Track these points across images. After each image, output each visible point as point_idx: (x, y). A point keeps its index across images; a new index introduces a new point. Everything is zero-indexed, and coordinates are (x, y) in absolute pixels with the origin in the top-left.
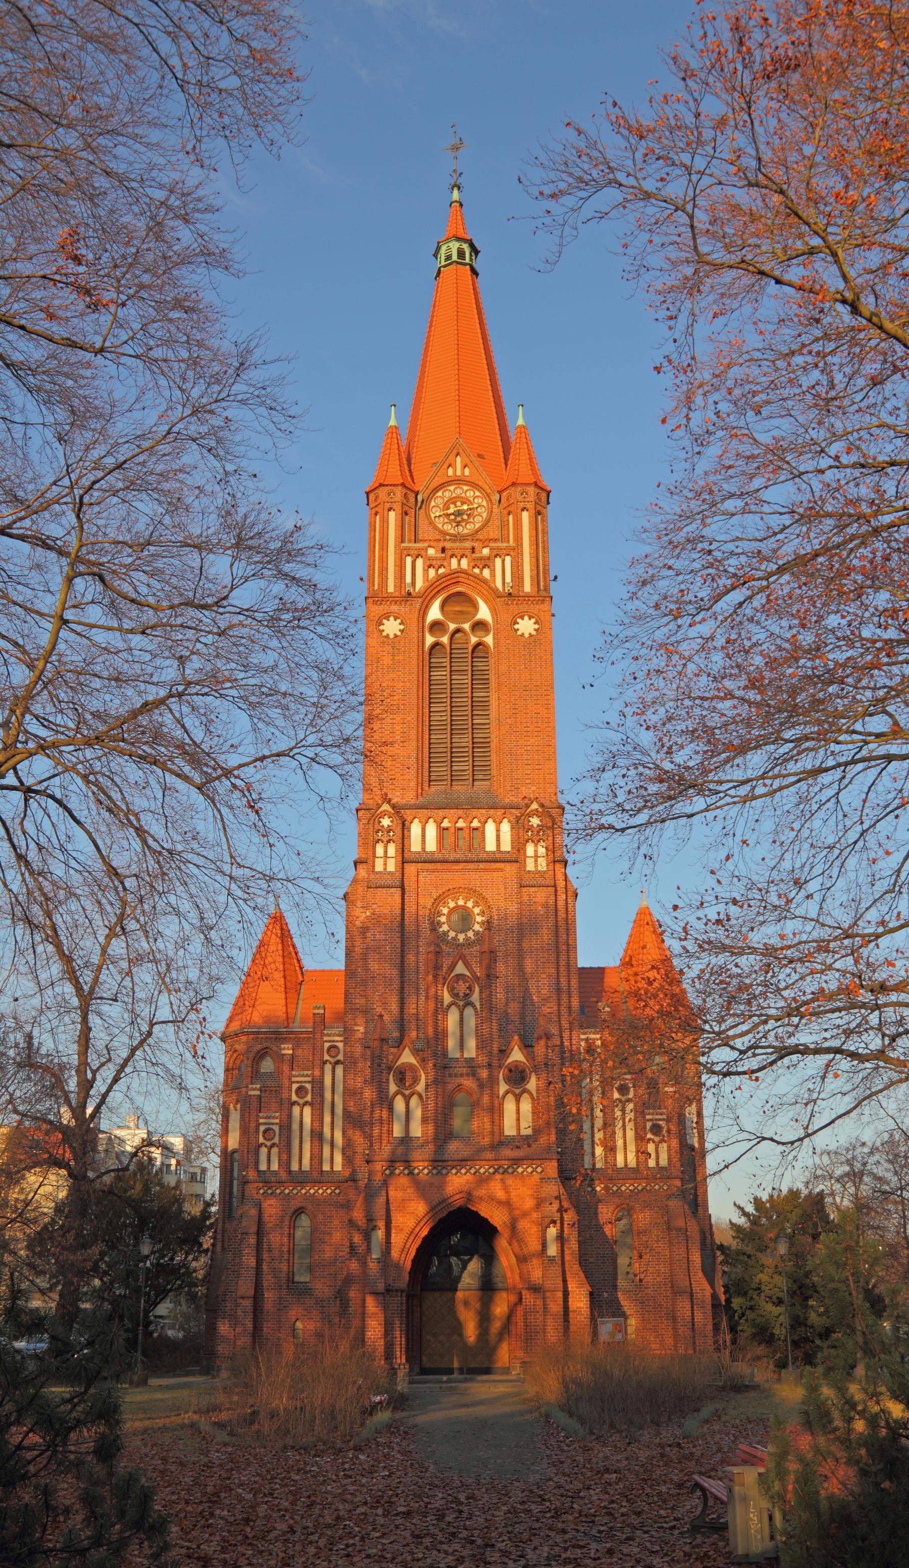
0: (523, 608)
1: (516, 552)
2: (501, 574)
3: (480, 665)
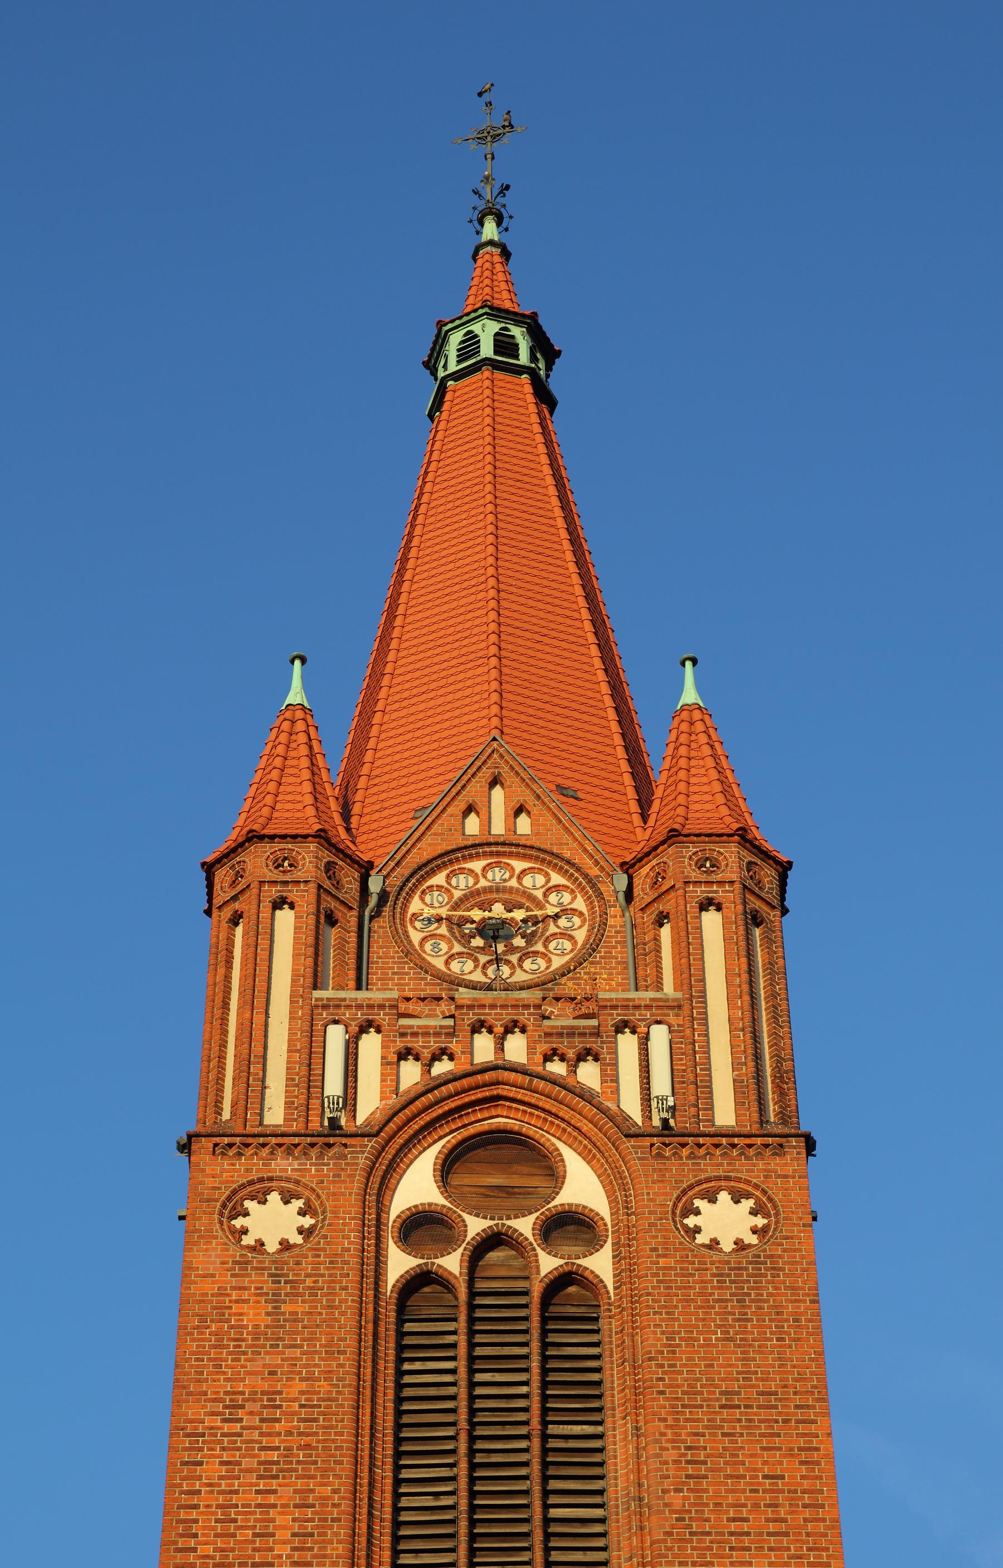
0: (709, 1168)
1: (687, 1014)
2: (637, 1074)
3: (570, 1343)
